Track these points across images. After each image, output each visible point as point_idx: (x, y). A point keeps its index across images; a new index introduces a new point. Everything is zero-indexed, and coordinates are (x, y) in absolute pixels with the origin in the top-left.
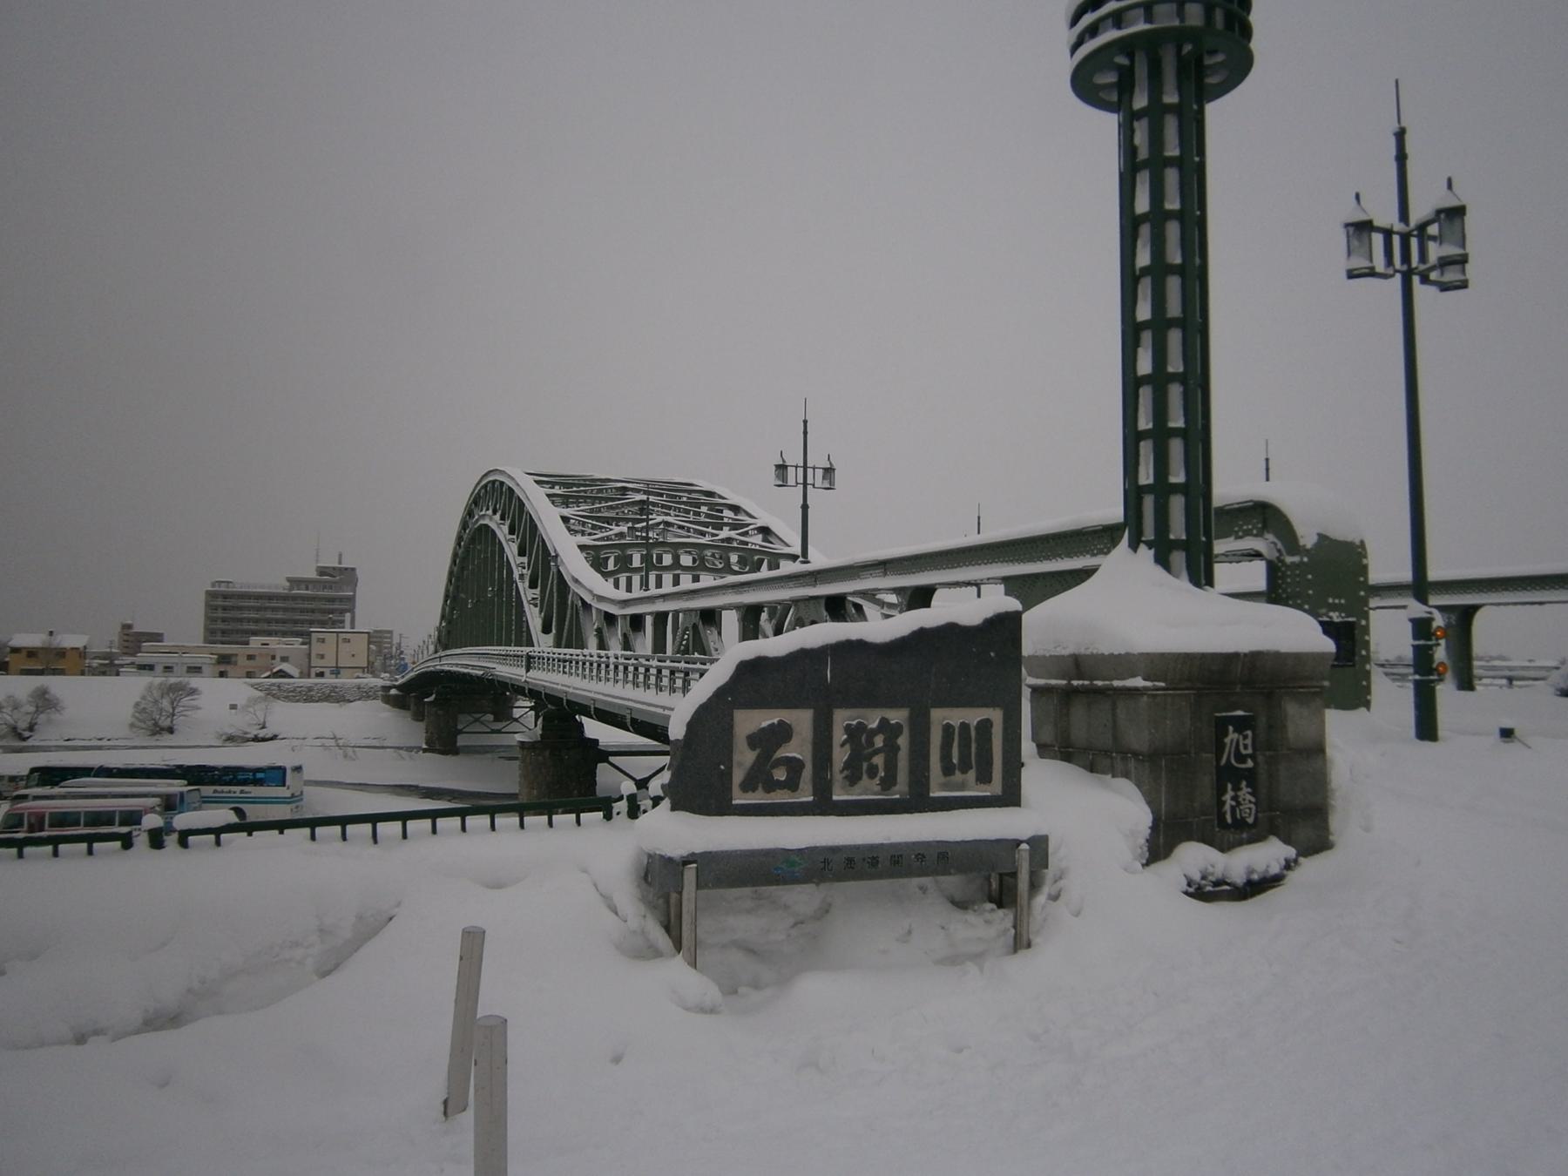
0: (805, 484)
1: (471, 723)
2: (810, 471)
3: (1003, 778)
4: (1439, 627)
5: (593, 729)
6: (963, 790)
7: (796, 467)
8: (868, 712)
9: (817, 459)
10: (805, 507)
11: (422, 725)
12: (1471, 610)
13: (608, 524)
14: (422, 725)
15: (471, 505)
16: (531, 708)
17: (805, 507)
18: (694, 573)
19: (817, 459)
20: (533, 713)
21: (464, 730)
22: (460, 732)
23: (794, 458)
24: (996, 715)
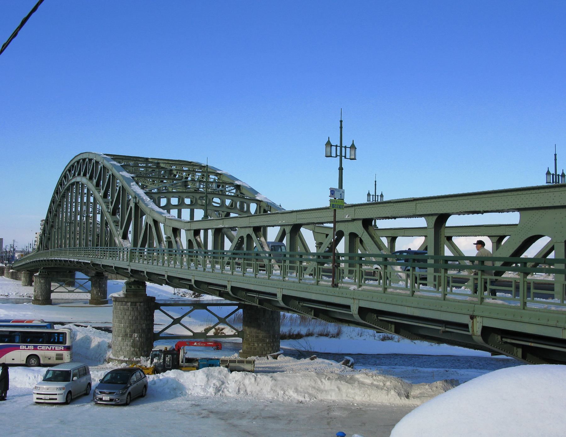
0: (341, 156)
1: (59, 287)
2: (343, 149)
3: (390, 321)
4: (218, 375)
5: (152, 288)
6: (203, 363)
7: (336, 146)
8: (328, 279)
9: (347, 143)
10: (341, 169)
11: (408, 250)
12: (152, 361)
13: (172, 186)
14: (408, 250)
15: (62, 178)
16: (89, 280)
17: (341, 169)
18: (192, 208)
19: (347, 143)
20: (52, 289)
21: (54, 291)
22: (53, 292)
23: (335, 141)
24: (21, 346)
